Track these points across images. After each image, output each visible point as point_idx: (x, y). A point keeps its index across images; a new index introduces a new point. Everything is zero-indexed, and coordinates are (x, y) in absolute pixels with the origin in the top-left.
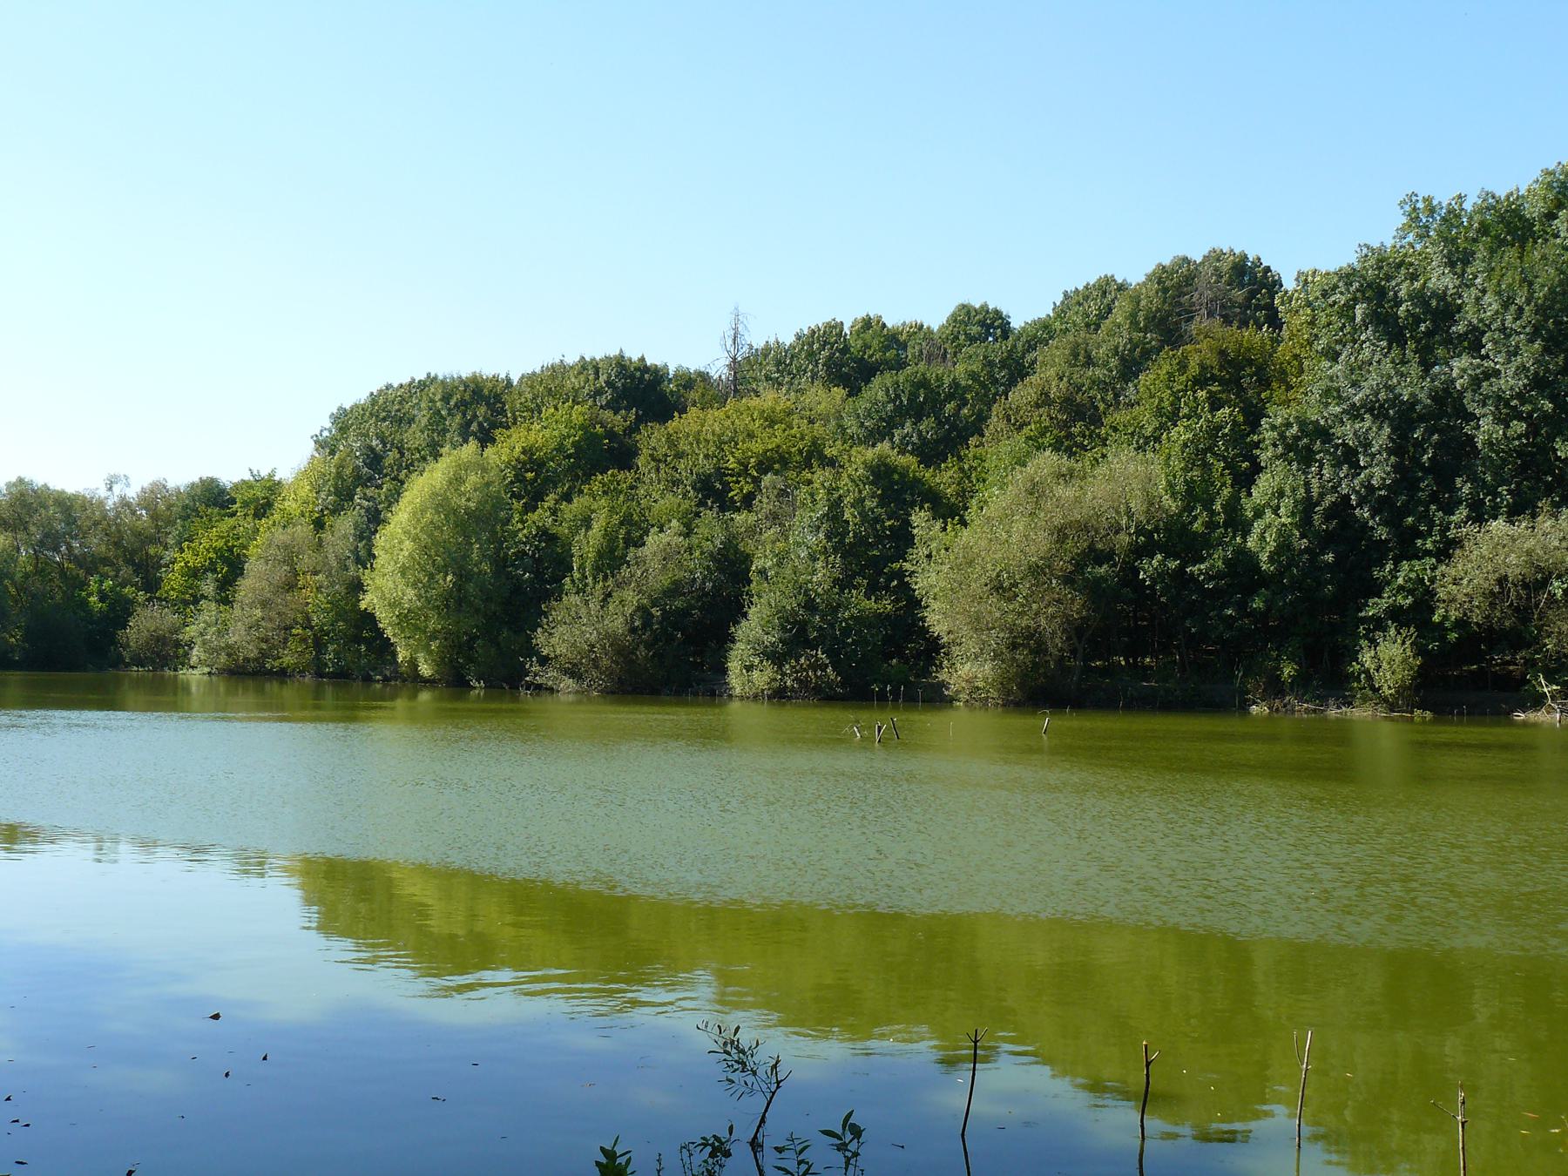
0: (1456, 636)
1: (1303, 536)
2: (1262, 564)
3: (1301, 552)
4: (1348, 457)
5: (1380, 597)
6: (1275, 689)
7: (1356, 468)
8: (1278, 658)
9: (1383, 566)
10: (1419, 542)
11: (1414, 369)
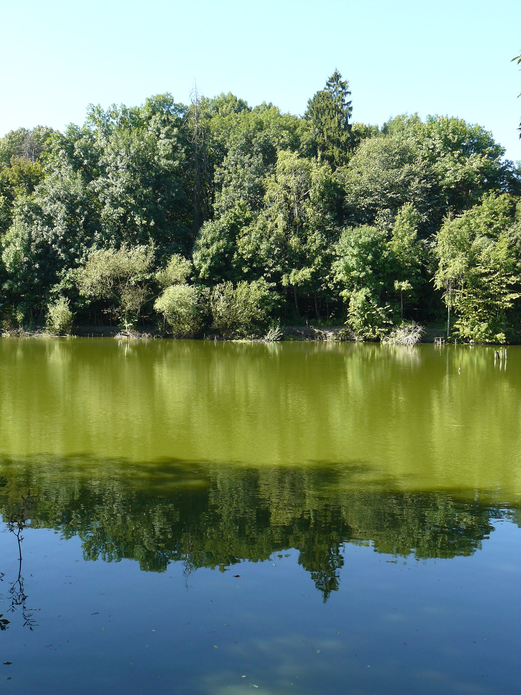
0: (90, 301)
1: (25, 256)
2: (6, 269)
3: (25, 263)
4: (49, 221)
5: (59, 284)
6: (15, 325)
7: (52, 226)
8: (15, 312)
9: (60, 271)
10: (76, 260)
11: (79, 181)
